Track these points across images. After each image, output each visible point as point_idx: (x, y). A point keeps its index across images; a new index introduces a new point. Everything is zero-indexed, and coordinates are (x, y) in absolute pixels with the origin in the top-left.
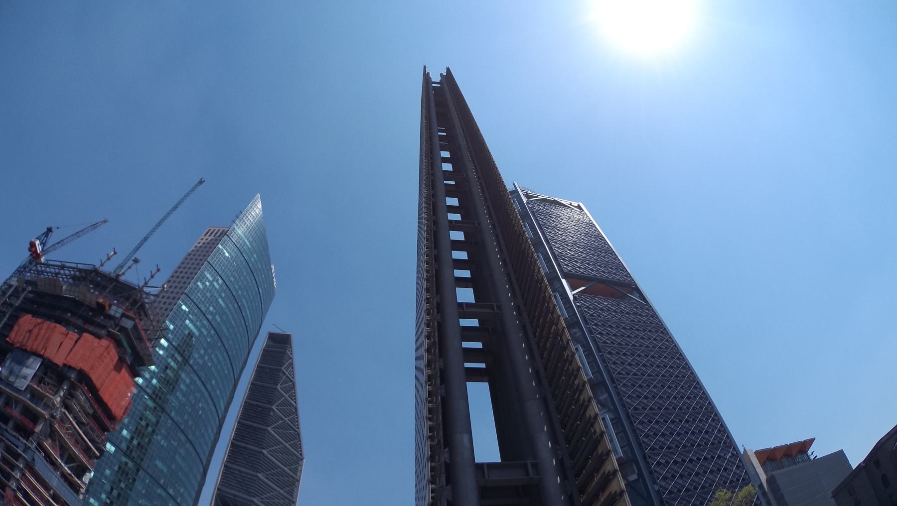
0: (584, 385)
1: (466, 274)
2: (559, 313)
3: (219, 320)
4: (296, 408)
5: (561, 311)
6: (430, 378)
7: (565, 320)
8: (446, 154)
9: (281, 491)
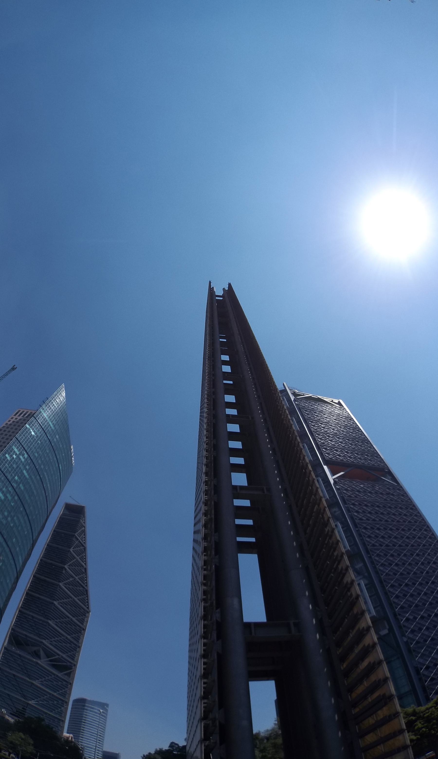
0: (342, 556)
1: (240, 461)
2: (321, 494)
3: (22, 488)
4: (86, 569)
5: (323, 492)
6: (206, 549)
7: (327, 500)
8: (225, 358)
9: (69, 637)
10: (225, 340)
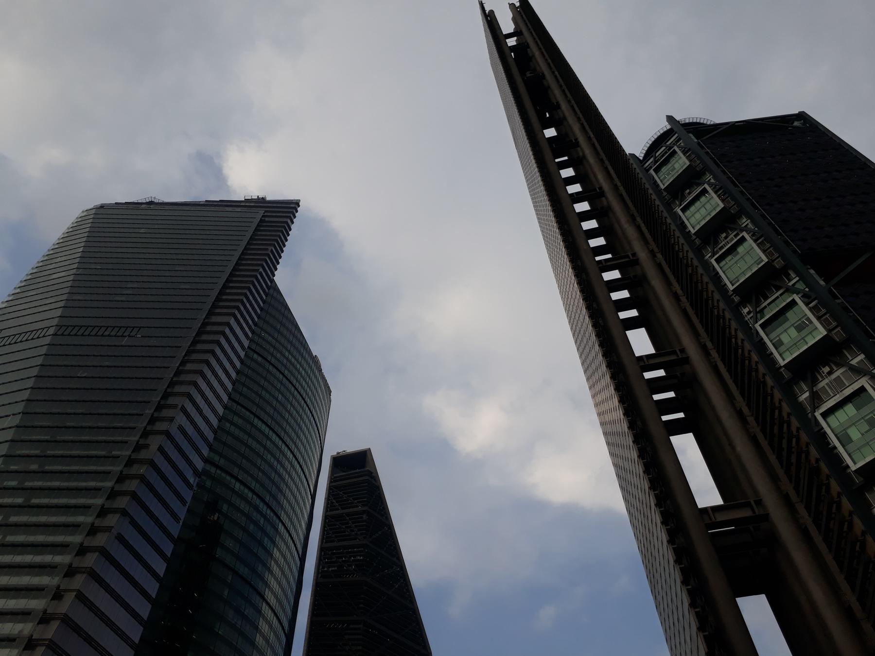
1: (624, 294)
10: (681, 415)
